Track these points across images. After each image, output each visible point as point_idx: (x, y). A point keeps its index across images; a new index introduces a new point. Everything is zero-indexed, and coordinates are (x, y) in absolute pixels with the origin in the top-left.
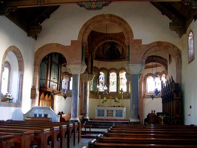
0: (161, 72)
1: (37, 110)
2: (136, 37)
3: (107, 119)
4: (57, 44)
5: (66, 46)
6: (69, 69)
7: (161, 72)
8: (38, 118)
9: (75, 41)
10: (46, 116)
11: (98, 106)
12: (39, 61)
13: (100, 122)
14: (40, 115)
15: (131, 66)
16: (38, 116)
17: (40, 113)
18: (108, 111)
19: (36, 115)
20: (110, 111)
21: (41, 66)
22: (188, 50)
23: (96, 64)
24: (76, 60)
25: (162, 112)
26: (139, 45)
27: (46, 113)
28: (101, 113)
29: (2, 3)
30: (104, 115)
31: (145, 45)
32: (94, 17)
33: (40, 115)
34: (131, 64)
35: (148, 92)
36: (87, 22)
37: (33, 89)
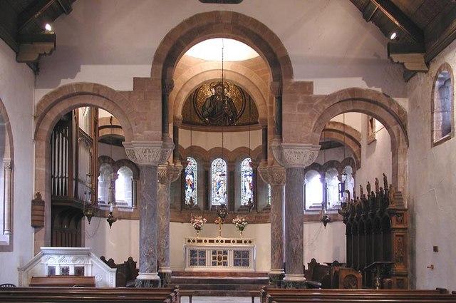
0: (340, 160)
1: (56, 257)
2: (297, 79)
3: (213, 273)
4: (95, 84)
5: (121, 92)
6: (133, 153)
7: (340, 160)
8: (58, 277)
9: (145, 78)
10: (80, 271)
11: (189, 241)
12: (47, 128)
13: (200, 281)
14: (65, 270)
15: (288, 147)
16: (58, 272)
17: (64, 264)
18: (214, 253)
19: (52, 270)
20: (220, 252)
21: (51, 143)
22: (432, 113)
23: (186, 138)
24: (149, 129)
25: (139, 221)
26: (305, 95)
27: (79, 263)
28: (196, 257)
29: (397, 38)
30: (205, 263)
31: (320, 97)
32: (191, 18)
33: (65, 270)
34: (288, 144)
35: (307, 208)
36: (173, 30)
37: (37, 202)
